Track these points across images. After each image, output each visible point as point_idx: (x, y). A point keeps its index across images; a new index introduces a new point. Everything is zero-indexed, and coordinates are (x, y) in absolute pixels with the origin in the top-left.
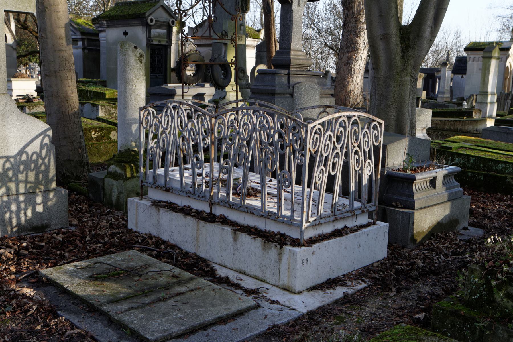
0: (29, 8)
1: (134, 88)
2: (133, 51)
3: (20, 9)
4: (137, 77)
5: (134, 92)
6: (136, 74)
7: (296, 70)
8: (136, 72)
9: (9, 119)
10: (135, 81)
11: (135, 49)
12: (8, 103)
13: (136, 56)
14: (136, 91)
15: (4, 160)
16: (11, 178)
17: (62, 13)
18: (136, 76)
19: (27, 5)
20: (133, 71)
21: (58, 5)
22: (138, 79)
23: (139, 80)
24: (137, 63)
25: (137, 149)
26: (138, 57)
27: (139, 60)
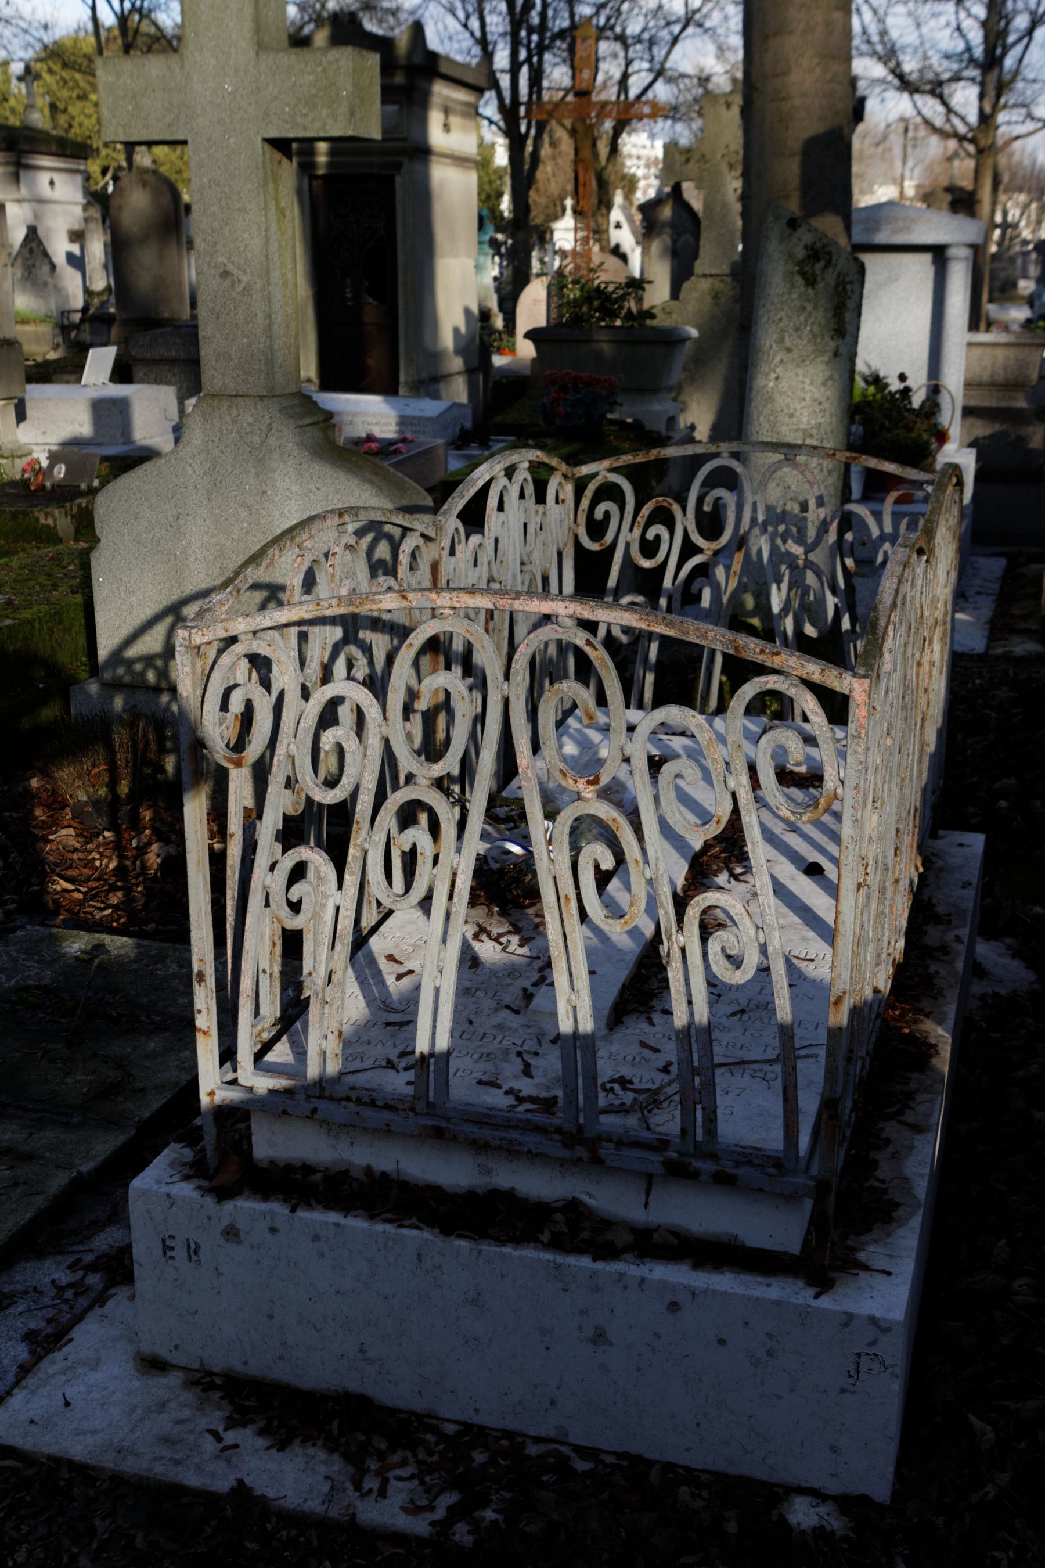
0: (330, 121)
1: (771, 384)
2: (782, 240)
3: (305, 129)
4: (788, 342)
5: (771, 399)
6: (782, 331)
7: (689, 995)
8: (785, 322)
9: (276, 475)
10: (778, 358)
11: (788, 231)
12: (275, 425)
13: (791, 256)
14: (777, 396)
15: (265, 594)
16: (158, 684)
17: (797, 102)
18: (781, 340)
19: (325, 112)
20: (776, 318)
21: (785, 73)
22: (789, 350)
23: (795, 355)
24: (793, 286)
25: (762, 621)
26: (801, 263)
27: (802, 273)
